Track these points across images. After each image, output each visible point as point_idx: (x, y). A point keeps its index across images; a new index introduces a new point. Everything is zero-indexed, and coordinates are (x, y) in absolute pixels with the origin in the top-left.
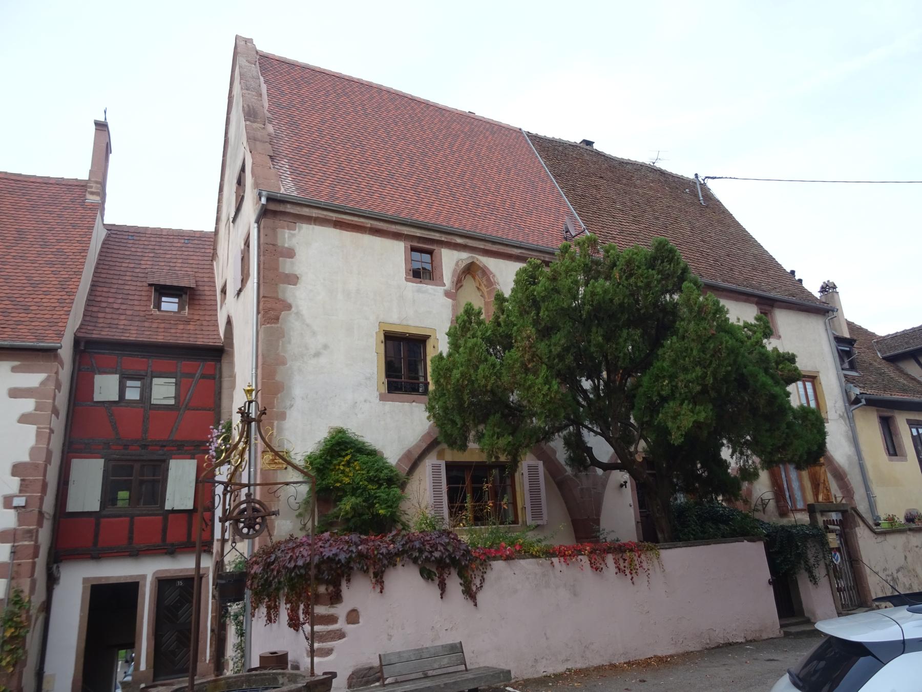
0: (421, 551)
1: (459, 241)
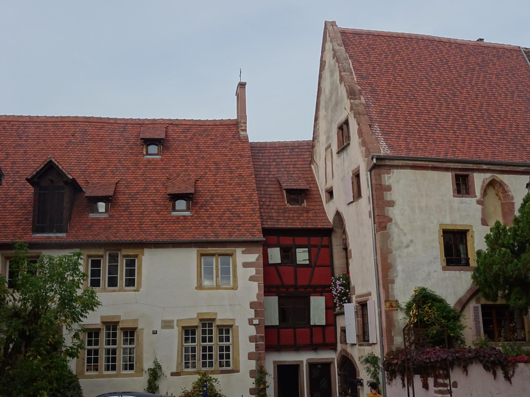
0: (484, 357)
1: (485, 167)
